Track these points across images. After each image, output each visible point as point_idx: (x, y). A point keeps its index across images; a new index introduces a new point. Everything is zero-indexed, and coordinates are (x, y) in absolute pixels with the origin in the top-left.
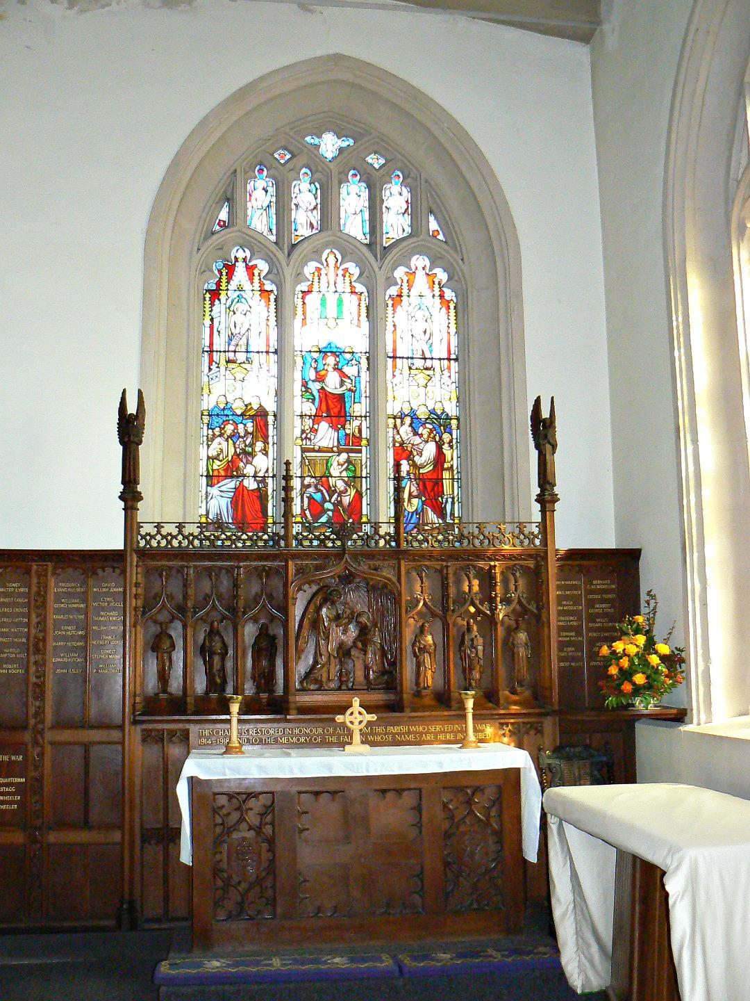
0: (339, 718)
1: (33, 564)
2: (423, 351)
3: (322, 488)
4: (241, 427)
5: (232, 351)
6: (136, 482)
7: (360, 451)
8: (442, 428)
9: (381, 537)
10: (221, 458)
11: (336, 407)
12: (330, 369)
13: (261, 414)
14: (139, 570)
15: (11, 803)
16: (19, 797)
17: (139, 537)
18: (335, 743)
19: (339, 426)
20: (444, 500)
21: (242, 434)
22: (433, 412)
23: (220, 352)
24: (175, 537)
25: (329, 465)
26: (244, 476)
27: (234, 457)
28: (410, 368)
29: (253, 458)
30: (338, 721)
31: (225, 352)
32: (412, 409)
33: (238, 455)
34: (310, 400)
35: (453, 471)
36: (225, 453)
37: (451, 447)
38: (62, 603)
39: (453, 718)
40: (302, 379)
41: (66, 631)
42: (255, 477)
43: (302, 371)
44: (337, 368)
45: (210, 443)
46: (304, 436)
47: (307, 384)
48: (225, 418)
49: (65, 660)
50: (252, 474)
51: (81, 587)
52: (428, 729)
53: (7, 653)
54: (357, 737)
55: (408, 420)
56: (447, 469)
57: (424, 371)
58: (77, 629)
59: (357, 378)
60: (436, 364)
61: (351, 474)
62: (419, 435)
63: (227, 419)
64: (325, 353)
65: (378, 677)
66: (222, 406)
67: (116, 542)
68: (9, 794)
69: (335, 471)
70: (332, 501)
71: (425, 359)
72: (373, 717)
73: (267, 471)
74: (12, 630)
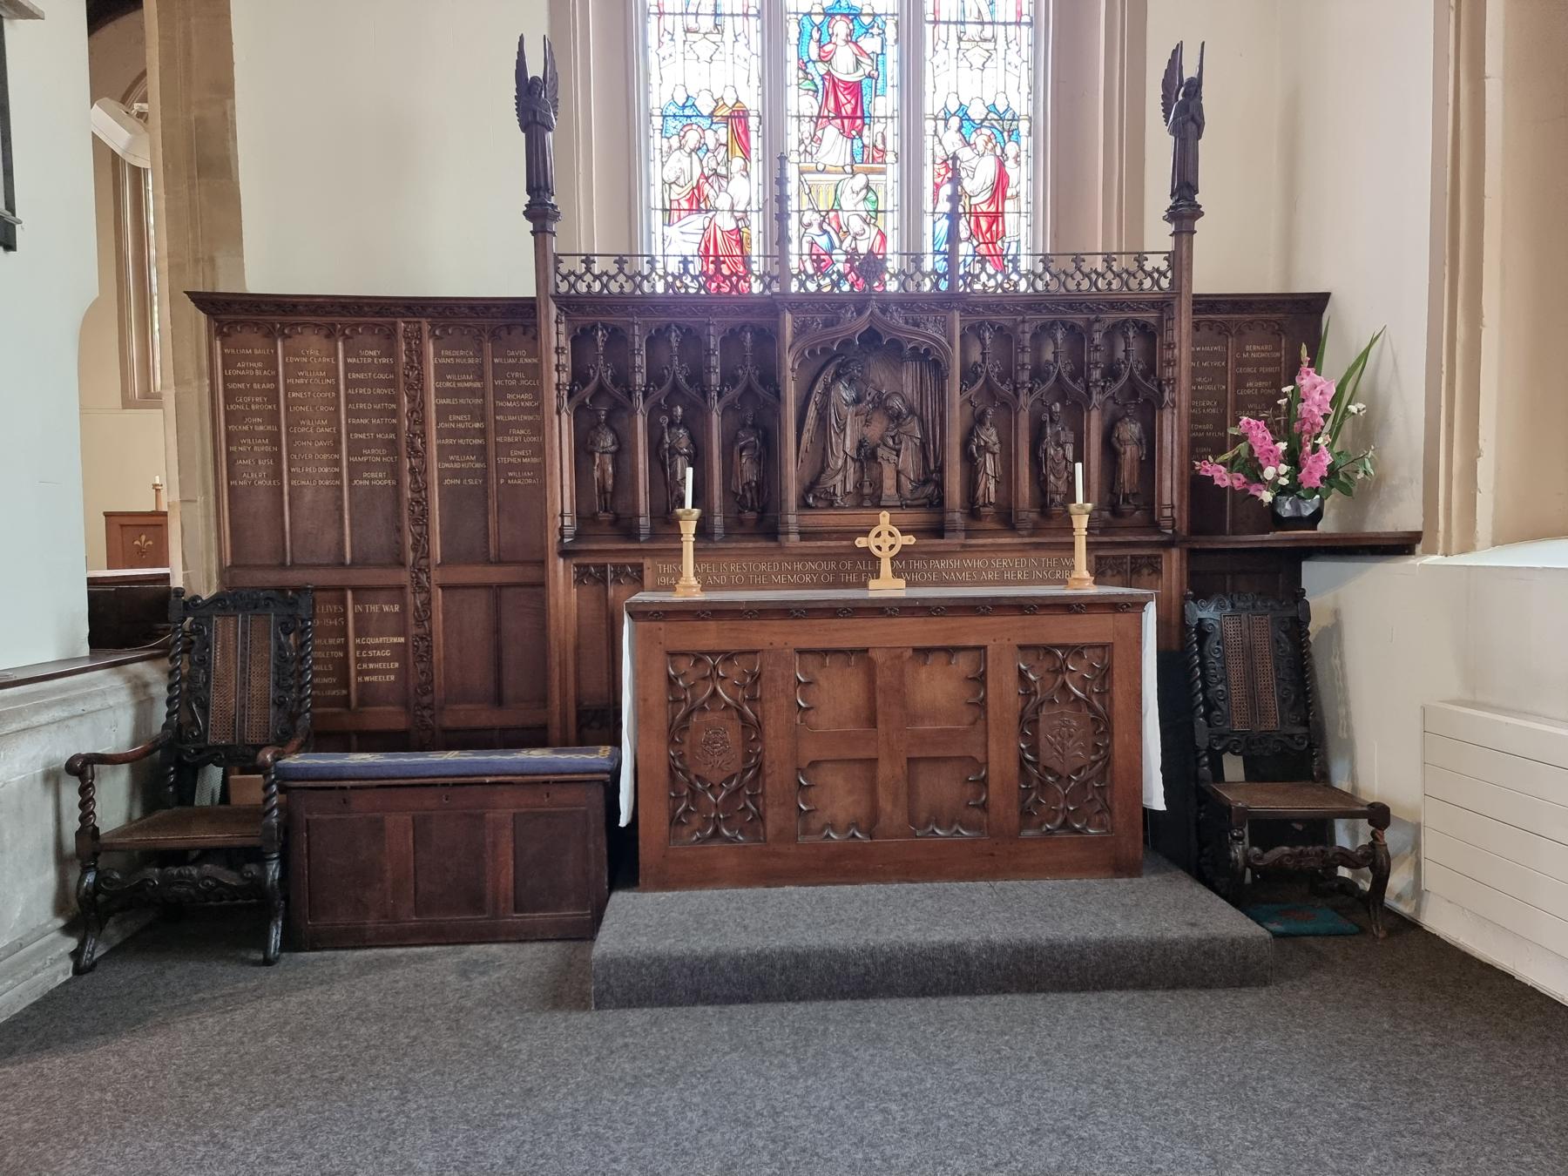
0: (861, 542)
1: (399, 320)
2: (979, 12)
3: (829, 229)
4: (709, 134)
5: (692, 14)
6: (548, 189)
7: (883, 172)
8: (1005, 134)
9: (924, 275)
10: (681, 182)
11: (849, 102)
12: (840, 42)
13: (738, 117)
14: (562, 328)
15: (386, 672)
16: (397, 665)
17: (559, 278)
18: (853, 583)
19: (854, 133)
20: (1006, 245)
21: (711, 147)
22: (992, 108)
23: (675, 14)
24: (613, 277)
25: (839, 193)
26: (717, 210)
27: (701, 181)
28: (960, 39)
29: (728, 182)
30: (859, 546)
31: (682, 14)
32: (961, 105)
33: (707, 179)
34: (811, 93)
35: (1019, 200)
36: (688, 174)
37: (1018, 163)
38: (446, 380)
39: (1028, 548)
40: (799, 59)
41: (456, 422)
42: (732, 210)
43: (798, 45)
44: (850, 39)
45: (664, 160)
46: (802, 148)
47: (806, 66)
48: (685, 121)
49: (457, 466)
50: (727, 207)
51: (475, 357)
52: (990, 564)
53: (368, 455)
54: (886, 567)
55: (954, 122)
56: (1012, 197)
57: (980, 44)
58: (473, 420)
59: (880, 58)
60: (1000, 29)
61: (870, 207)
62: (969, 145)
63: (689, 122)
64: (832, 16)
65: (916, 488)
66: (681, 101)
67: (522, 285)
68: (384, 659)
69: (848, 202)
70: (844, 248)
71: (982, 23)
72: (910, 540)
73: (749, 203)
74: (374, 421)
